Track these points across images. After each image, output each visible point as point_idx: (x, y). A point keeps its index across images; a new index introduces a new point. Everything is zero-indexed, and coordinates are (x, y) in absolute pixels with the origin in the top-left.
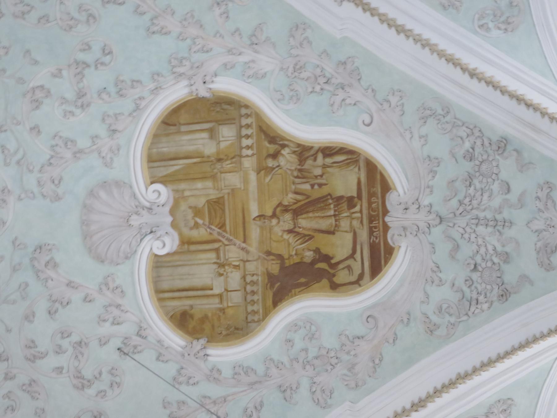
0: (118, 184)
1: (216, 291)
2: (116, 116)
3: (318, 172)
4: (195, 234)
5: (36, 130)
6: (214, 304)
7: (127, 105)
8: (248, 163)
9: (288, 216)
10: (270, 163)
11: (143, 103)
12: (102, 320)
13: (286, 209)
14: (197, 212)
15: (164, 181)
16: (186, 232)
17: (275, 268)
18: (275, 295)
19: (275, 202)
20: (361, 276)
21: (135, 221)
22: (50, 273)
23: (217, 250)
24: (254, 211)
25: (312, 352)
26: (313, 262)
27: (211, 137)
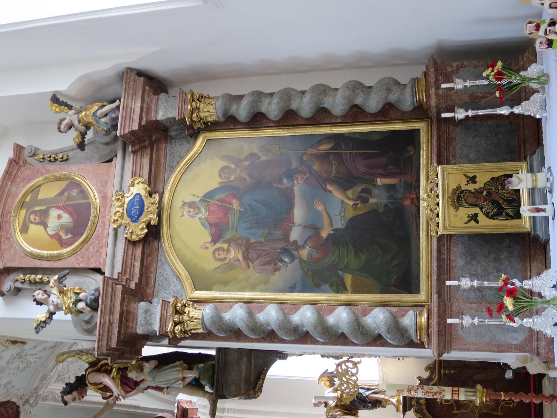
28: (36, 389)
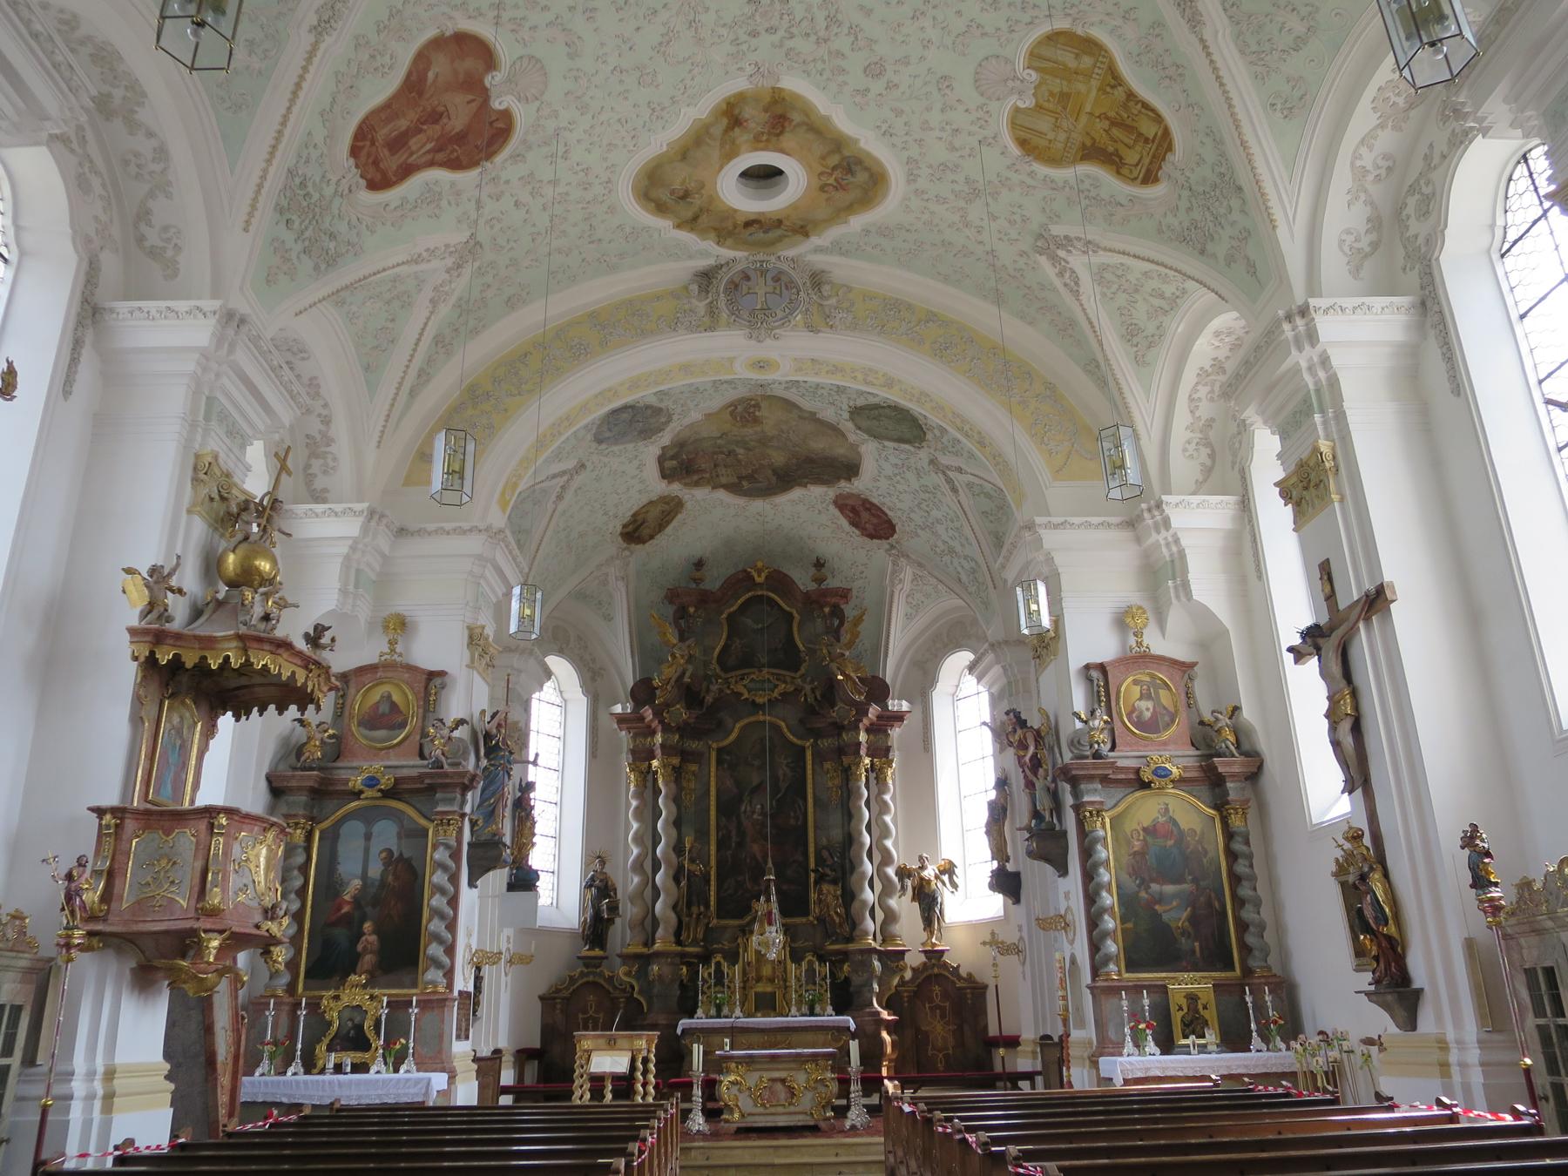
0: (1007, 61)
1: (1048, 137)
2: (1017, 21)
3: (1136, 112)
4: (1046, 105)
5: (959, 13)
6: (1047, 143)
7: (1026, 18)
8: (1095, 83)
9: (1107, 123)
10: (1108, 89)
11: (1037, 21)
12: (972, 123)
13: (1107, 118)
14: (1051, 94)
15: (1036, 69)
16: (1041, 101)
17: (1088, 143)
18: (1083, 155)
19: (1103, 111)
20: (1136, 179)
21: (1010, 84)
22: (948, 91)
23: (1057, 119)
24: (1088, 108)
25: (1093, 194)
26: (1111, 154)
27: (1076, 58)
28: (908, 556)
